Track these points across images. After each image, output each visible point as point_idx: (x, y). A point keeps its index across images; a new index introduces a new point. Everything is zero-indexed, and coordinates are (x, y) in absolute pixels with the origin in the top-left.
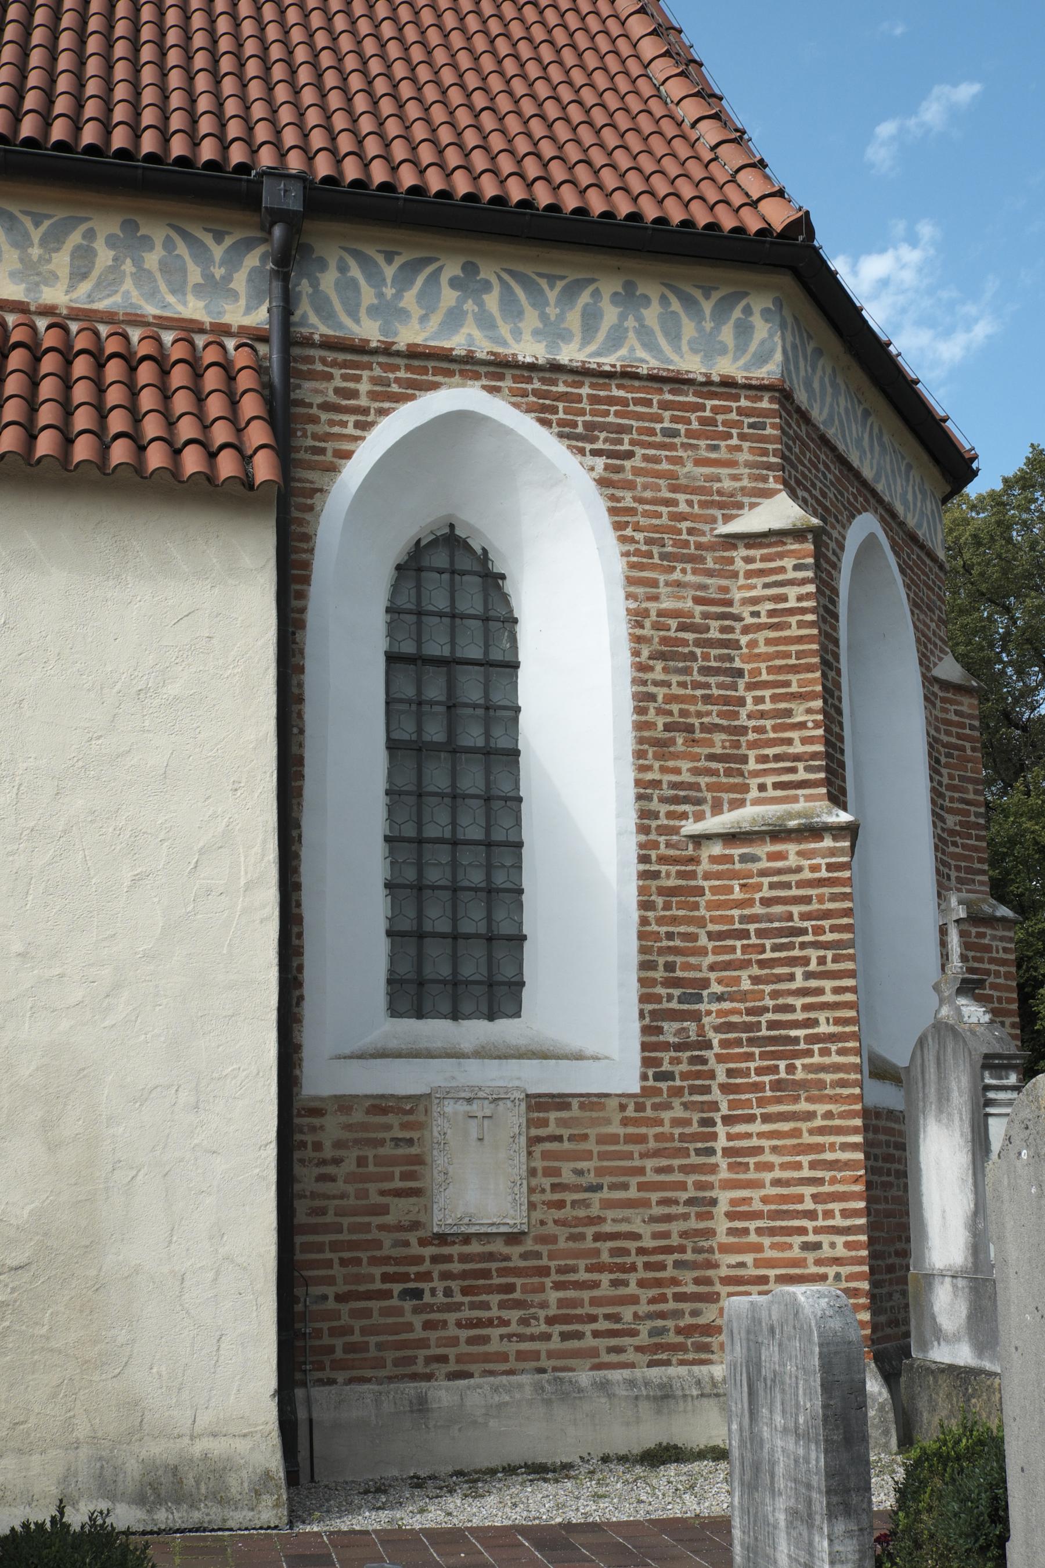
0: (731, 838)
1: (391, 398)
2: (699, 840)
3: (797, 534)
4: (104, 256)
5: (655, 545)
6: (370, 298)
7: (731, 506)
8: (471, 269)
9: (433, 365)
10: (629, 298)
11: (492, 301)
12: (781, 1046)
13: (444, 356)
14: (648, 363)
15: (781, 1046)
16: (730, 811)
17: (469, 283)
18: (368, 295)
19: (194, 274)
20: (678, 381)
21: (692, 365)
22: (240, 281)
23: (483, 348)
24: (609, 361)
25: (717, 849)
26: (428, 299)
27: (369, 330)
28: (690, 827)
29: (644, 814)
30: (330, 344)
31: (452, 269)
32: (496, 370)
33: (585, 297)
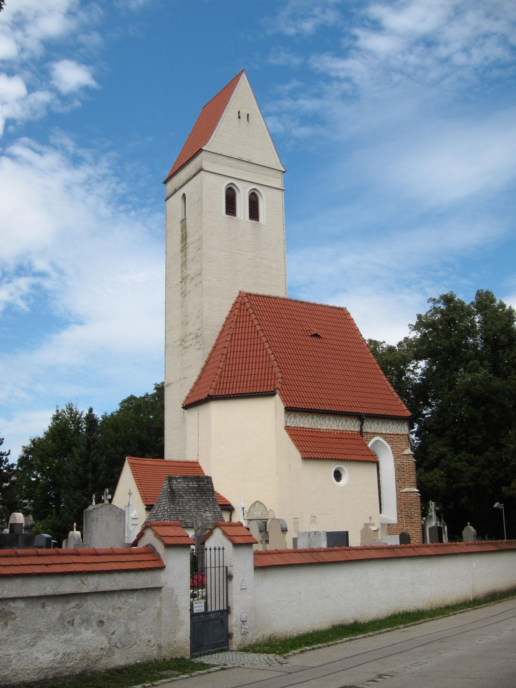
0: (405, 492)
1: (371, 439)
2: (402, 492)
3: (411, 455)
4: (344, 423)
5: (397, 456)
6: (370, 427)
7: (403, 450)
8: (295, 415)
9: (375, 434)
10: (347, 421)
11: (380, 425)
12: (411, 518)
13: (376, 433)
14: (395, 433)
15: (411, 518)
16: (53, 548)
17: (295, 417)
18: (368, 426)
19: (302, 421)
20: (398, 435)
21: (399, 432)
22: (357, 425)
23: (380, 432)
24: (391, 433)
25: (404, 494)
26: (374, 426)
27: (369, 430)
28: (401, 491)
29: (397, 489)
30: (365, 433)
31: (376, 422)
32: (381, 434)
33: (341, 421)
